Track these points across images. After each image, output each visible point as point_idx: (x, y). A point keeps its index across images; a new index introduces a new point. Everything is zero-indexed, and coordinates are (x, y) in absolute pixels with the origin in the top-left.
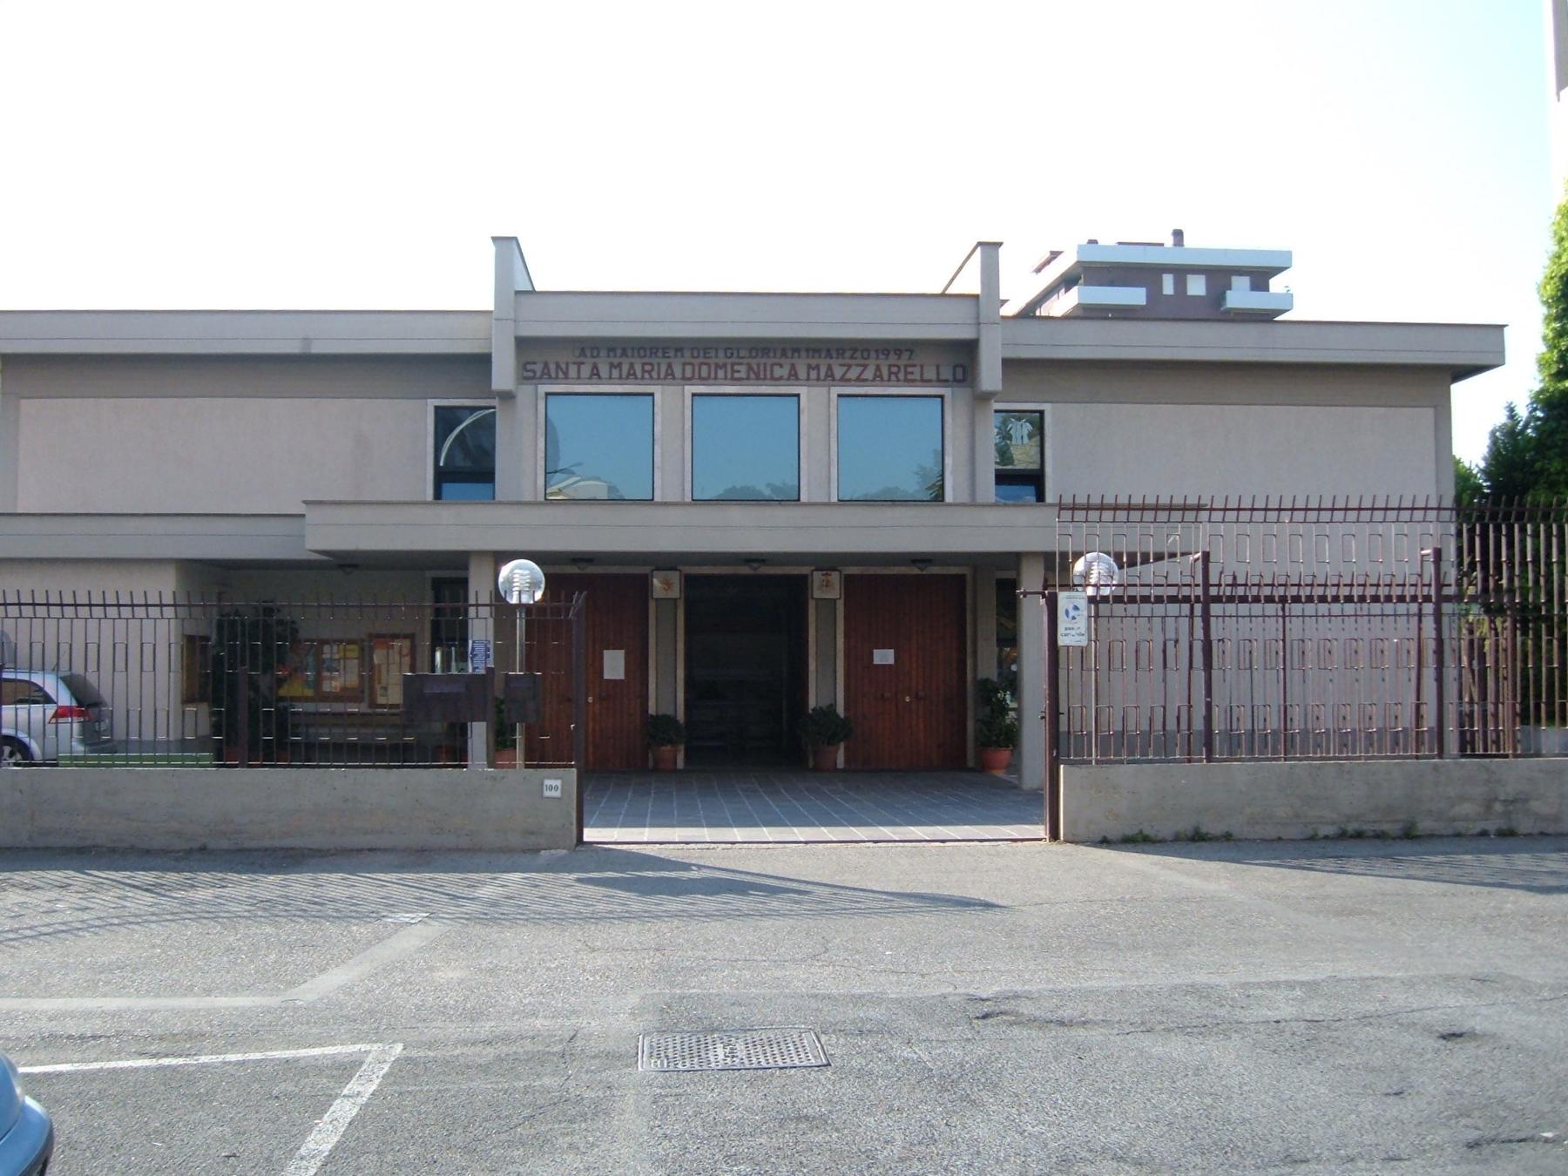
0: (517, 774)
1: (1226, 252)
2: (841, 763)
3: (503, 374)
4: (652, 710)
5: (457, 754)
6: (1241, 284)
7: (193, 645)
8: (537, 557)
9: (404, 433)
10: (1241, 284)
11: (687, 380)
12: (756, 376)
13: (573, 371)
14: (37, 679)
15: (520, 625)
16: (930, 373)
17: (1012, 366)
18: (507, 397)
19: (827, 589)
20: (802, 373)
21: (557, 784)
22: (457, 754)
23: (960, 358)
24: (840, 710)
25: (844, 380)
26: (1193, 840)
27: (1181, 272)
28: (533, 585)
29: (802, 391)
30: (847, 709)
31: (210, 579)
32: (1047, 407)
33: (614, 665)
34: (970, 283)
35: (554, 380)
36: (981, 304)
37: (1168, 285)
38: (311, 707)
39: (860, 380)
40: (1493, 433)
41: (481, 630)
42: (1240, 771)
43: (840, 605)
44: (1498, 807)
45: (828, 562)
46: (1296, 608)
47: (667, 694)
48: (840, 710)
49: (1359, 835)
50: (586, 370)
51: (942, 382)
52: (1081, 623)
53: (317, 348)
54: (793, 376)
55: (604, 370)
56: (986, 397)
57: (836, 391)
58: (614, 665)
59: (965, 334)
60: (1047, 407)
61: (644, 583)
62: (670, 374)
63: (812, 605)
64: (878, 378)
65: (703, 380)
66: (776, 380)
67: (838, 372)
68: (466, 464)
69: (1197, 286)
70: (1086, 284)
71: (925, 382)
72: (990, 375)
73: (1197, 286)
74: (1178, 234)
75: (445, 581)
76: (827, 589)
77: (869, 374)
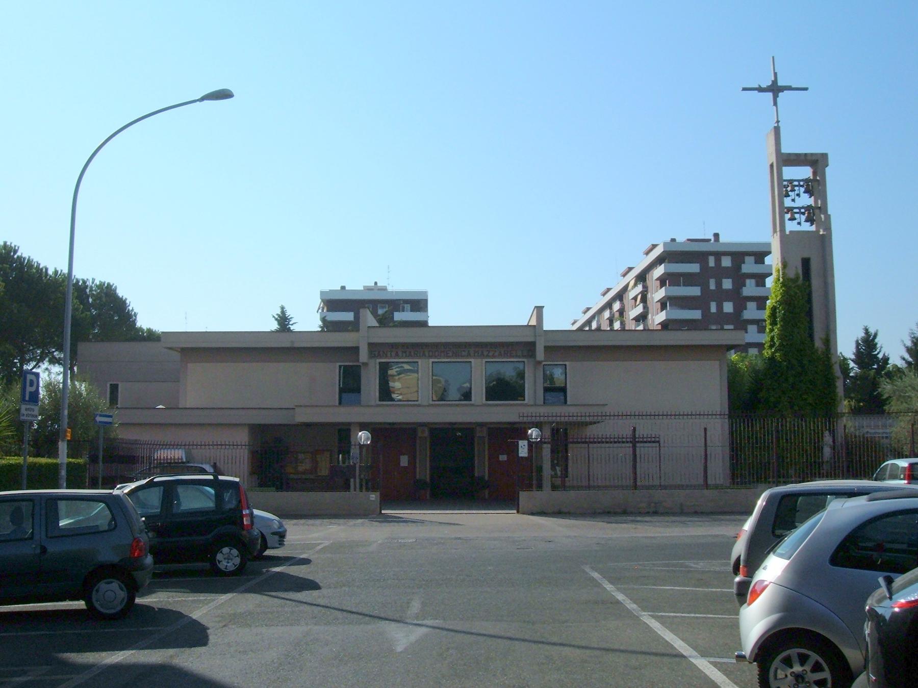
0: (363, 495)
1: (741, 244)
2: (487, 496)
3: (364, 356)
4: (418, 477)
5: (347, 487)
6: (749, 260)
7: (253, 454)
8: (393, 400)
9: (329, 375)
10: (749, 260)
11: (430, 357)
12: (456, 355)
13: (389, 354)
14: (204, 466)
15: (364, 450)
16: (520, 353)
17: (547, 349)
18: (366, 364)
19: (481, 433)
20: (472, 354)
21: (374, 497)
22: (347, 487)
23: (529, 348)
24: (486, 478)
25: (488, 356)
26: (559, 513)
27: (718, 255)
28: (367, 439)
29: (472, 360)
30: (489, 477)
31: (258, 430)
32: (567, 363)
33: (404, 461)
34: (533, 322)
35: (381, 358)
36: (536, 329)
37: (712, 262)
38: (295, 477)
39: (494, 356)
40: (857, 342)
41: (355, 451)
42: (572, 494)
43: (486, 439)
44: (653, 505)
45: (482, 425)
46: (591, 445)
47: (423, 472)
48: (486, 478)
49: (609, 513)
50: (393, 354)
51: (524, 356)
52: (526, 450)
53: (296, 345)
54: (469, 355)
55: (400, 353)
56: (540, 362)
57: (484, 360)
58: (404, 461)
59: (531, 339)
60: (567, 363)
61: (414, 431)
62: (424, 355)
63: (476, 440)
64: (500, 355)
65: (436, 357)
66: (462, 356)
67: (485, 353)
68: (350, 384)
69: (726, 262)
70: (669, 262)
71: (517, 356)
72: (540, 355)
73: (726, 262)
74: (716, 236)
75: (344, 432)
76: (481, 433)
77: (497, 354)
